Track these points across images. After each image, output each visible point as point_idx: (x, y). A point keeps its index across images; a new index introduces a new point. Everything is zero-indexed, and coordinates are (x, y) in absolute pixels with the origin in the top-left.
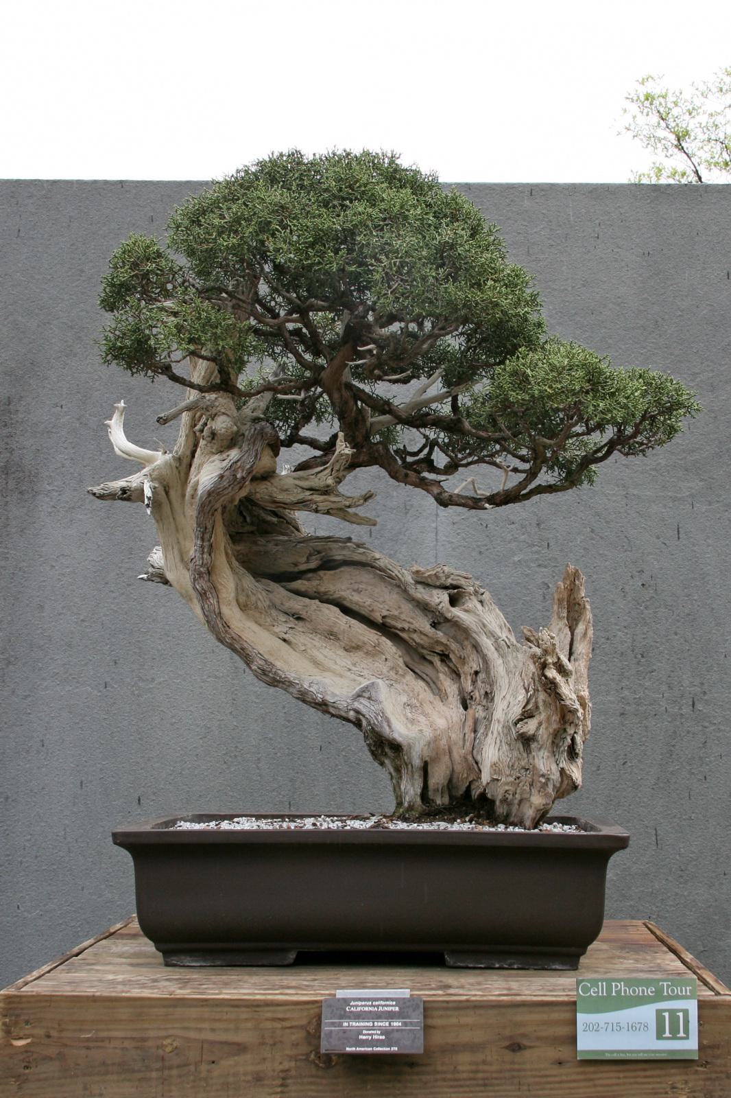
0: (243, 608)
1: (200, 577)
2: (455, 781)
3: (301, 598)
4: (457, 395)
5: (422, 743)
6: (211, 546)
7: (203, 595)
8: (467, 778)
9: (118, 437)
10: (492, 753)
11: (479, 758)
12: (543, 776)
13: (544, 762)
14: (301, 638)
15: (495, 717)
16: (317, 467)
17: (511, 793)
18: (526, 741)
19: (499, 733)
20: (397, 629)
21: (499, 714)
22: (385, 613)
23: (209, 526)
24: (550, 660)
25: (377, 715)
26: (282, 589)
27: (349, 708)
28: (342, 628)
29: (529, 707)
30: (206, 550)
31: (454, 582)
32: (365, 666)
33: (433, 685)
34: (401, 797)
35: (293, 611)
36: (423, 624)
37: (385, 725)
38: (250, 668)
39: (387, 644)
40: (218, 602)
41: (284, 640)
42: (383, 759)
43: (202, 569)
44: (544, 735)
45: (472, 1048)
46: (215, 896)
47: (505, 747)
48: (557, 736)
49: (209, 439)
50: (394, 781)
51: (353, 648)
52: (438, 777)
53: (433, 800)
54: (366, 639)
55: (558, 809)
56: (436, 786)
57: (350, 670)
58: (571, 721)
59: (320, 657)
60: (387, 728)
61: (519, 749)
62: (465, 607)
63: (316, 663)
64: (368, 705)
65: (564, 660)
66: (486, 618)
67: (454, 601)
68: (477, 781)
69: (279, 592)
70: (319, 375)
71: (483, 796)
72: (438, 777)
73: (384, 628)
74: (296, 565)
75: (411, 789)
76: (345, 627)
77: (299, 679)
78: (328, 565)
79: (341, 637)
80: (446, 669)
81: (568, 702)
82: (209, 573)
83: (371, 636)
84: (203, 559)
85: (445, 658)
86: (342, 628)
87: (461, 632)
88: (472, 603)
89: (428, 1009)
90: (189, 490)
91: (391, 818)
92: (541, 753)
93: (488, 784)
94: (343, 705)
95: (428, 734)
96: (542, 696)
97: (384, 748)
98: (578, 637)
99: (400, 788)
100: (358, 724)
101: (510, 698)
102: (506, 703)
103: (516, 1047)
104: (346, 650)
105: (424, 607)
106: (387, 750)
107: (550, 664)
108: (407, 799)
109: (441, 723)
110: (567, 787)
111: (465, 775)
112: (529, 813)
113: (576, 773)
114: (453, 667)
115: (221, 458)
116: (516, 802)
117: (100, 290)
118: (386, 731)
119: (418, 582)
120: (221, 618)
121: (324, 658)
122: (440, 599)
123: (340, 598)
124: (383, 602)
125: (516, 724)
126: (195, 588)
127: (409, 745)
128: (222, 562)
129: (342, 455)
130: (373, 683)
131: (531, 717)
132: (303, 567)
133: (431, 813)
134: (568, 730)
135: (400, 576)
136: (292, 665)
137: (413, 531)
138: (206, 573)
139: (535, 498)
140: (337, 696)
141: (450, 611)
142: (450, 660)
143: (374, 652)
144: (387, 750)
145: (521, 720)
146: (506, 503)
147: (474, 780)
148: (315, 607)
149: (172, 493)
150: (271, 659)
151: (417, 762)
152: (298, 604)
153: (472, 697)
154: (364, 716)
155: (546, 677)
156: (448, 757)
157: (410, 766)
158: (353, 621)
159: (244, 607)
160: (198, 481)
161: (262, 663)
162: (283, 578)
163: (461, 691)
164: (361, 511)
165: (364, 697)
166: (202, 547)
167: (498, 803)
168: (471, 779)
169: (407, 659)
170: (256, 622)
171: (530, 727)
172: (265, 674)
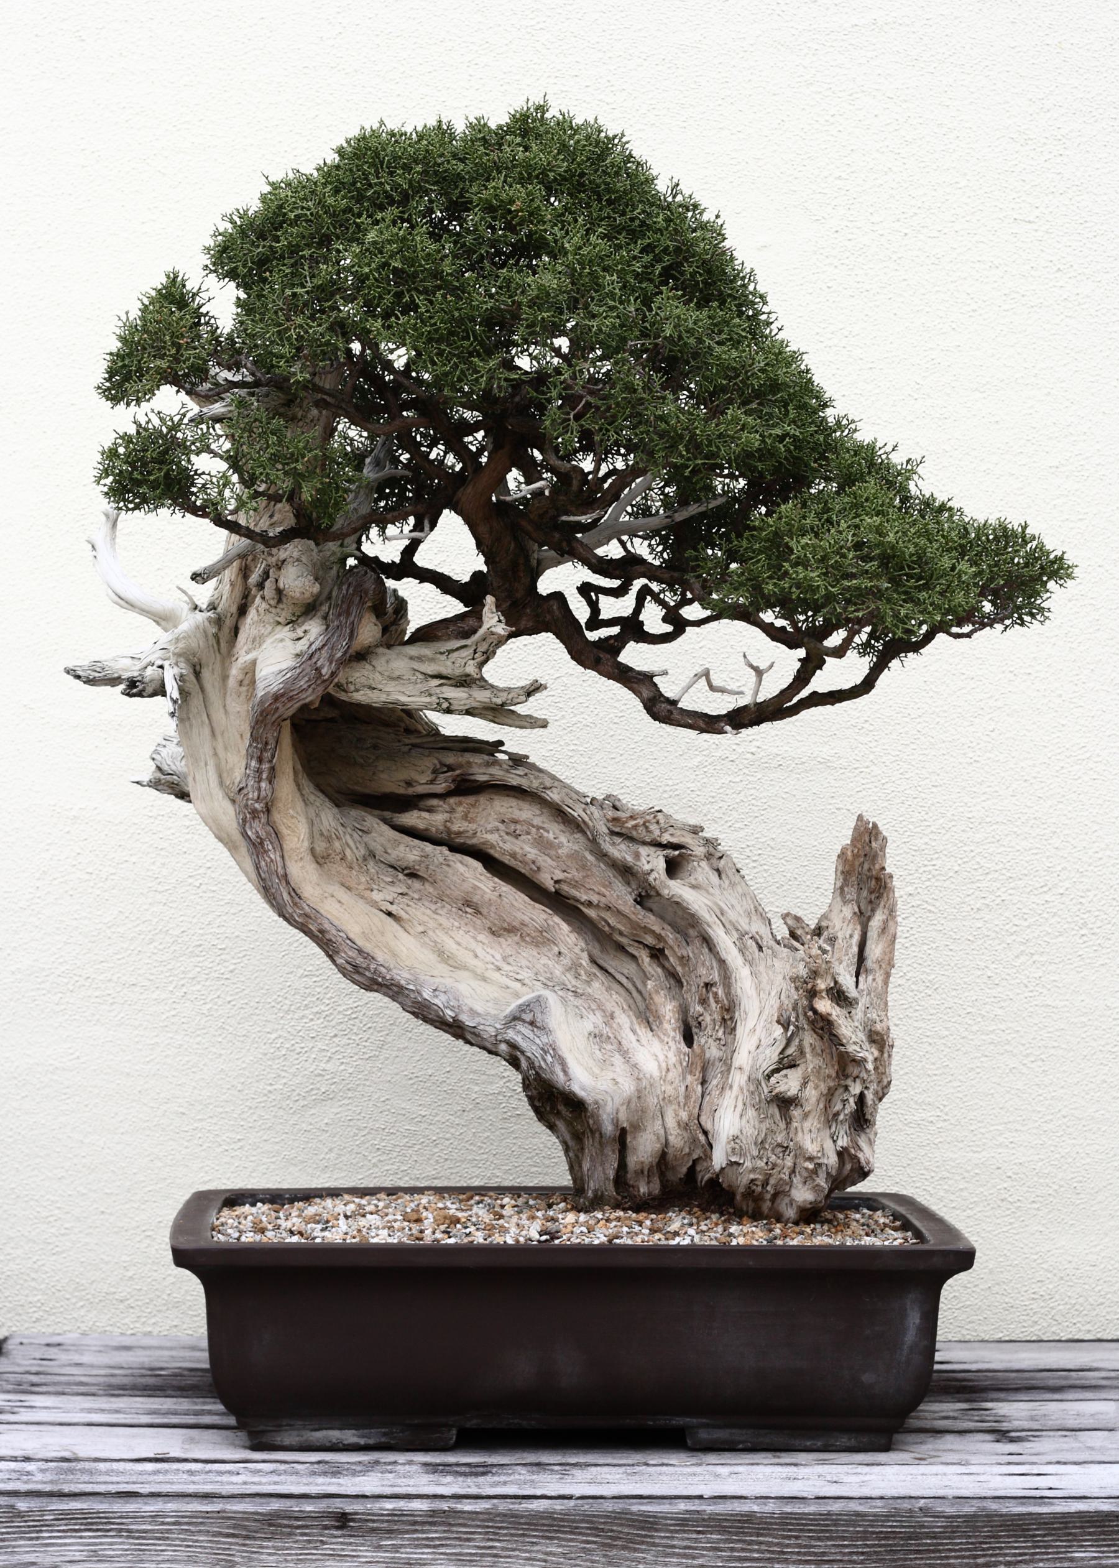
0: (321, 861)
1: (254, 818)
2: (670, 1157)
3: (417, 842)
5: (618, 1101)
6: (273, 769)
8: (689, 1154)
11: (708, 1126)
12: (810, 1159)
14: (419, 913)
15: (736, 1063)
16: (449, 639)
17: (759, 1183)
18: (785, 1103)
19: (742, 1089)
20: (578, 901)
21: (743, 1057)
22: (559, 875)
23: (272, 742)
24: (822, 985)
25: (546, 1052)
26: (385, 828)
27: (499, 1038)
28: (487, 897)
29: (789, 1051)
30: (264, 776)
31: (673, 840)
32: (524, 963)
34: (582, 1179)
35: (404, 865)
36: (622, 896)
37: (558, 1069)
38: (334, 961)
39: (562, 928)
40: (283, 857)
41: (389, 914)
42: (552, 1119)
43: (257, 805)
44: (811, 1095)
47: (751, 1113)
49: (273, 602)
50: (571, 1154)
51: (505, 930)
52: (644, 1148)
53: (633, 1187)
54: (526, 919)
56: (638, 1167)
57: (499, 969)
58: (854, 1074)
59: (450, 945)
60: (561, 1074)
61: (772, 1116)
62: (692, 880)
63: (443, 956)
64: (531, 1036)
65: (847, 981)
67: (673, 868)
68: (705, 1160)
70: (454, 493)
71: (714, 1182)
72: (644, 1148)
73: (558, 901)
74: (409, 784)
76: (494, 896)
77: (416, 981)
79: (484, 911)
80: (659, 970)
81: (851, 1048)
82: (268, 810)
83: (536, 914)
84: (259, 789)
85: (657, 954)
86: (487, 897)
87: (687, 924)
90: (235, 672)
92: (807, 1125)
93: (722, 1169)
94: (489, 1031)
95: (628, 1086)
96: (809, 1039)
98: (873, 934)
99: (580, 1166)
100: (514, 1062)
101: (756, 1040)
102: (754, 1042)
104: (493, 933)
105: (626, 872)
106: (561, 1107)
107: (821, 991)
108: (592, 1184)
111: (687, 1150)
114: (670, 968)
115: (294, 635)
116: (768, 1196)
117: (98, 372)
118: (560, 1078)
119: (612, 833)
120: (288, 883)
121: (455, 946)
122: (653, 863)
123: (483, 843)
124: (554, 856)
125: (769, 1077)
126: (244, 834)
127: (596, 1102)
128: (286, 787)
129: (493, 633)
130: (538, 999)
131: (793, 1066)
132: (420, 789)
134: (851, 1089)
135: (587, 819)
136: (406, 953)
139: (805, 714)
140: (479, 1015)
141: (668, 887)
142: (667, 958)
143: (542, 939)
144: (561, 1107)
145: (777, 1070)
146: (758, 722)
147: (700, 1158)
148: (441, 860)
149: (206, 674)
150: (368, 947)
151: (608, 1128)
152: (410, 851)
153: (700, 1023)
154: (523, 1052)
155: (815, 1012)
156: (660, 1122)
157: (597, 1135)
158: (506, 888)
159: (320, 859)
160: (254, 663)
161: (353, 954)
163: (684, 1010)
164: (520, 709)
165: (524, 1021)
166: (259, 771)
167: (738, 1197)
168: (695, 1156)
169: (596, 952)
170: (343, 885)
171: (789, 1083)
172: (358, 972)
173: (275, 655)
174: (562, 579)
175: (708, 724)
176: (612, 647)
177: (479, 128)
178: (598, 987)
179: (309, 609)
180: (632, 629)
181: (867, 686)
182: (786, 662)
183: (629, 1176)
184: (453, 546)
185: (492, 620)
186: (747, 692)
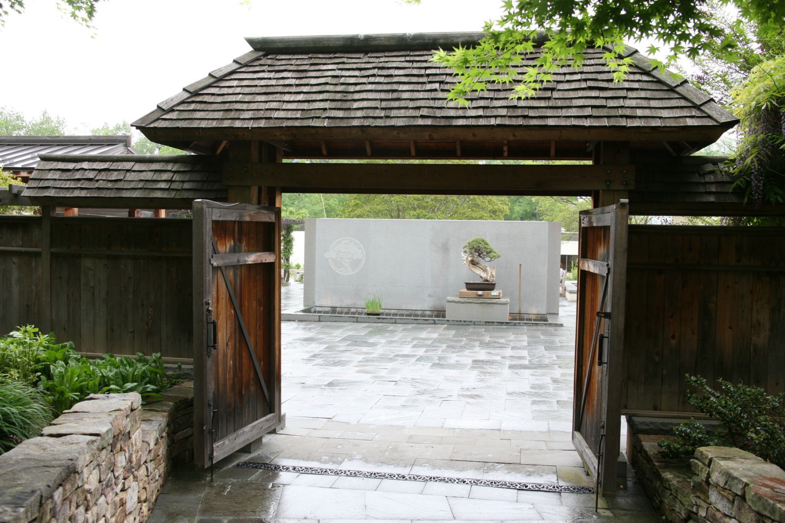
4: (610, 319)
9: (463, 255)
46: (470, 286)
66: (488, 269)
97: (481, 277)
101: (490, 274)
136: (475, 271)
138: (469, 265)
162: (474, 265)
173: (470, 259)
184: (477, 254)
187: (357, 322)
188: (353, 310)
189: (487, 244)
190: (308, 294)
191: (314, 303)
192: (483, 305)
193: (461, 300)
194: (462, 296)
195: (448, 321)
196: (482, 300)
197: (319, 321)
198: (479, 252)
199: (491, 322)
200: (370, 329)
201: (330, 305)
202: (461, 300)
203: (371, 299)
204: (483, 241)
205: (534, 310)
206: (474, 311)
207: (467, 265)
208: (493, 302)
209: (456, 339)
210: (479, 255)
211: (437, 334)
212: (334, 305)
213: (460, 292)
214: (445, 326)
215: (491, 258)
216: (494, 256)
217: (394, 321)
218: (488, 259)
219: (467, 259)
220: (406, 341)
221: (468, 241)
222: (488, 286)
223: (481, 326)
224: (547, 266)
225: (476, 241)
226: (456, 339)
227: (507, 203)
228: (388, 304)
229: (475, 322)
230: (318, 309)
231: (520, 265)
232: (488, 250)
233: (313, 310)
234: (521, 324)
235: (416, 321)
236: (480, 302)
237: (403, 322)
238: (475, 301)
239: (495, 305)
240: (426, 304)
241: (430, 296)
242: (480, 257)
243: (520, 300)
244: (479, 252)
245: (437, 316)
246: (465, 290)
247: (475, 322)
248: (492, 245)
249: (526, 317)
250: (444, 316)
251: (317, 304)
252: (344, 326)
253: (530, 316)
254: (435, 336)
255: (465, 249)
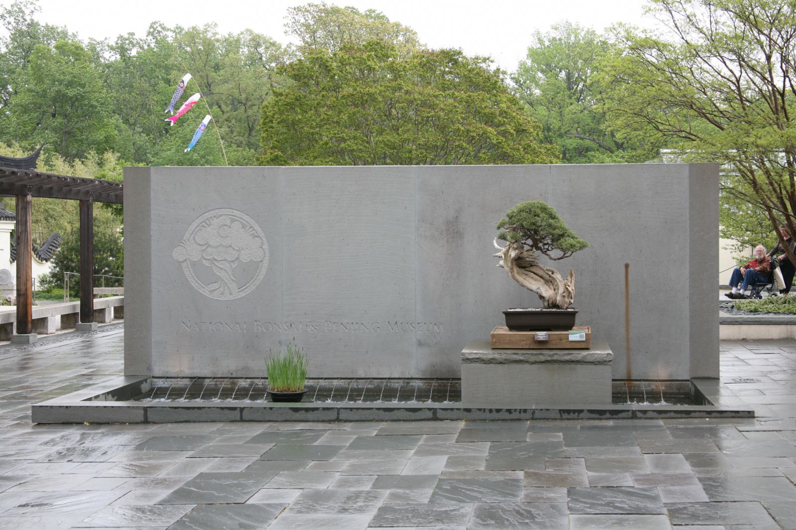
7: (511, 273)
10: (559, 298)
13: (567, 300)
14: (527, 279)
18: (564, 296)
21: (560, 292)
33: (549, 286)
36: (548, 277)
39: (542, 280)
44: (566, 296)
45: (555, 340)
46: (517, 321)
48: (568, 296)
52: (550, 302)
55: (570, 307)
66: (558, 276)
67: (552, 273)
69: (523, 270)
72: (550, 302)
73: (541, 277)
75: (546, 304)
78: (532, 266)
83: (539, 278)
85: (551, 282)
87: (554, 279)
88: (555, 274)
89: (549, 335)
91: (543, 308)
97: (541, 297)
101: (561, 290)
103: (561, 340)
105: (548, 274)
109: (551, 293)
110: (570, 303)
112: (565, 308)
113: (572, 301)
122: (550, 273)
124: (541, 273)
133: (549, 308)
137: (544, 262)
138: (512, 269)
143: (540, 281)
152: (527, 272)
159: (518, 273)
162: (524, 268)
171: (564, 294)
173: (513, 254)
174: (540, 245)
175: (555, 260)
176: (546, 252)
177: (398, 25)
178: (546, 285)
179: (516, 249)
180: (548, 250)
181: (571, 255)
182: (562, 253)
183: (485, 464)
184: (530, 242)
185: (534, 250)
186: (559, 257)
187: (242, 420)
188: (243, 383)
189: (553, 218)
190: (135, 350)
191: (149, 369)
192: (550, 366)
193: (496, 355)
194: (496, 344)
195: (468, 410)
196: (547, 355)
197: (146, 422)
198: (534, 234)
199: (574, 411)
200: (266, 447)
201: (187, 372)
202: (496, 355)
203: (282, 358)
204: (544, 209)
205: (661, 371)
206: (527, 383)
207: (507, 269)
208: (570, 359)
209: (498, 477)
210: (535, 246)
211: (444, 459)
212: (198, 372)
213: (493, 336)
214: (462, 425)
215: (564, 251)
216: (572, 246)
217: (333, 415)
218: (556, 253)
219: (506, 254)
220: (357, 495)
221: (509, 212)
222: (558, 318)
223: (551, 424)
224: (688, 265)
225: (529, 211)
226: (498, 477)
227: (557, 153)
228: (325, 365)
229: (533, 413)
230: (160, 383)
231: (627, 266)
232: (557, 232)
233: (145, 387)
234: (649, 415)
235: (388, 415)
236: (542, 358)
237: (356, 417)
238: (531, 355)
239: (579, 366)
240: (410, 365)
241: (420, 344)
242: (538, 248)
243: (628, 349)
244: (534, 234)
245: (439, 395)
246: (504, 330)
247: (534, 412)
248: (565, 221)
249: (644, 387)
250: (456, 395)
251: (157, 371)
252: (202, 438)
253: (653, 386)
254: (438, 465)
255: (502, 230)
